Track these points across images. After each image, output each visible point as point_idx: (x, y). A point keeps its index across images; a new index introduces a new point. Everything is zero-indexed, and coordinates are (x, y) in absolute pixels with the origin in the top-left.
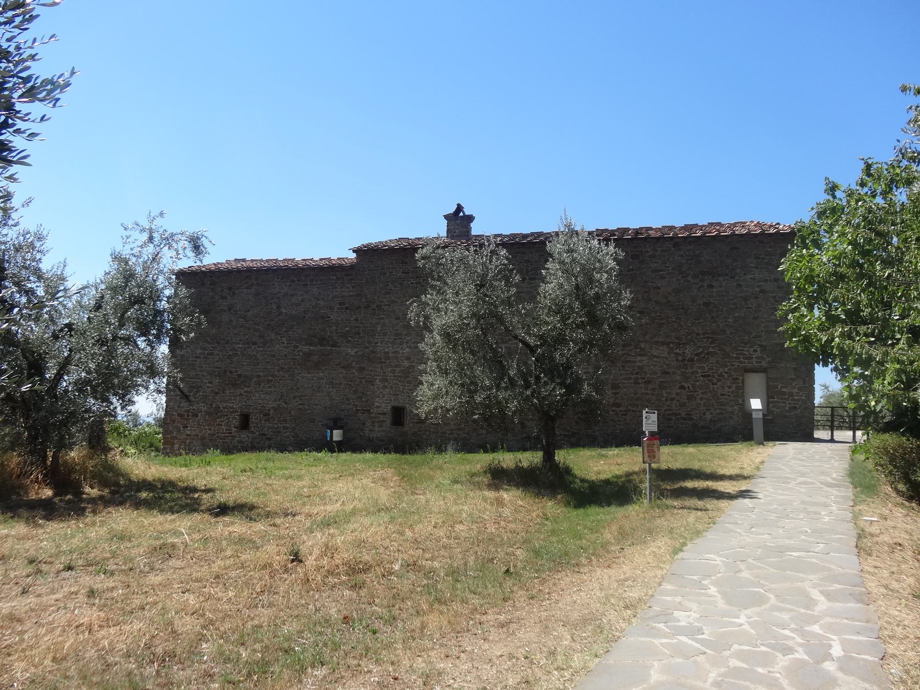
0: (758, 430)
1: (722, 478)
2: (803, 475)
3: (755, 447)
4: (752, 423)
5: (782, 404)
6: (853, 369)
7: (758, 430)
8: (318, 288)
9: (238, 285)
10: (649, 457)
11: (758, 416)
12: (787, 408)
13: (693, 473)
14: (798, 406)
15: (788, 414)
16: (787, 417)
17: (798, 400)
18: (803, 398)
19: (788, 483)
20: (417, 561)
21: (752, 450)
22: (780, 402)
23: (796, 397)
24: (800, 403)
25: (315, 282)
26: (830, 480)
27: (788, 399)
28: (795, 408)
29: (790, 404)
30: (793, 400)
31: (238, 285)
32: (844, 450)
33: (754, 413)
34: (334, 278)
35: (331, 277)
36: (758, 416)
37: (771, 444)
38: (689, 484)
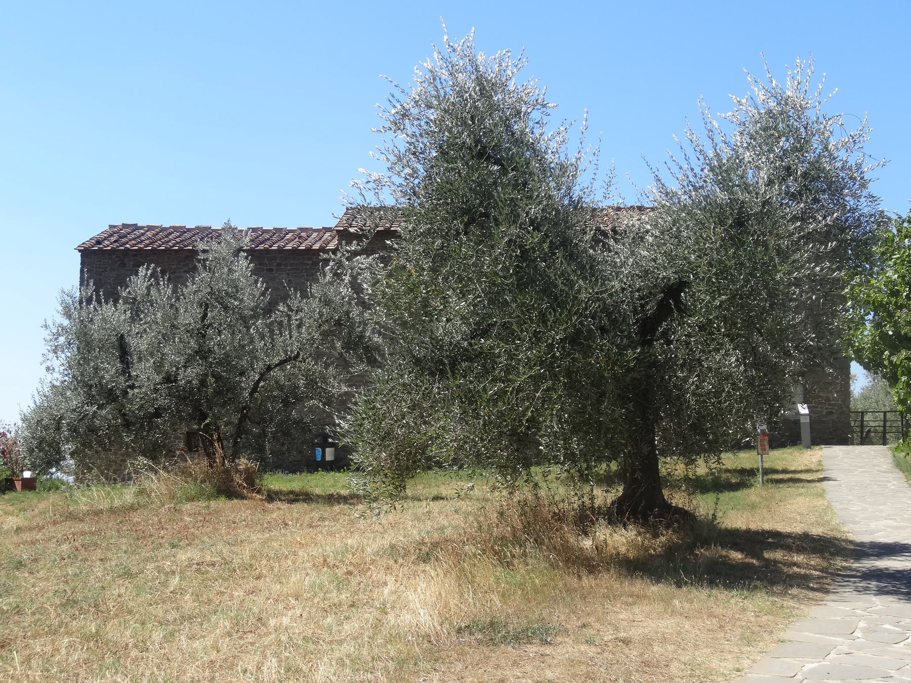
0: (806, 434)
1: (801, 472)
2: (860, 467)
3: (804, 451)
4: (800, 428)
5: (819, 409)
6: (901, 379)
7: (806, 434)
8: (288, 274)
9: (173, 267)
10: (762, 449)
11: (805, 421)
12: (824, 413)
13: (769, 471)
14: (834, 411)
15: (825, 419)
16: (824, 422)
17: (834, 405)
18: (840, 402)
19: (853, 472)
20: (409, 610)
21: (802, 453)
22: (817, 407)
23: (832, 402)
24: (836, 408)
25: (283, 267)
26: (883, 469)
27: (825, 404)
28: (831, 413)
29: (827, 408)
30: (830, 405)
31: (173, 267)
32: (883, 450)
33: (802, 418)
34: (310, 262)
35: (306, 262)
36: (805, 421)
37: (817, 448)
38: (776, 476)
